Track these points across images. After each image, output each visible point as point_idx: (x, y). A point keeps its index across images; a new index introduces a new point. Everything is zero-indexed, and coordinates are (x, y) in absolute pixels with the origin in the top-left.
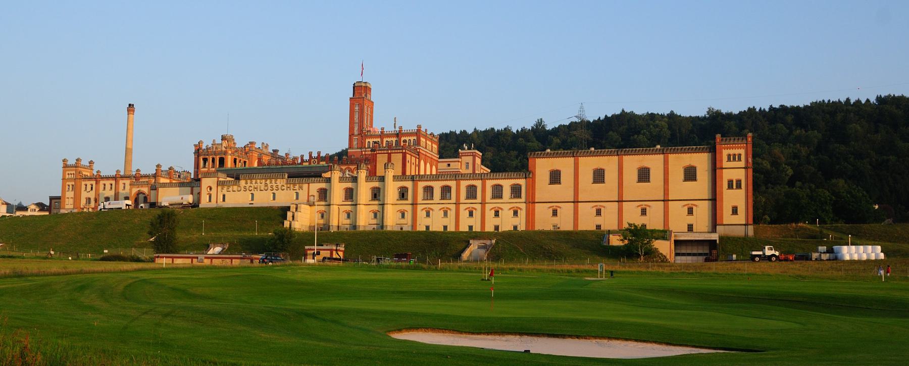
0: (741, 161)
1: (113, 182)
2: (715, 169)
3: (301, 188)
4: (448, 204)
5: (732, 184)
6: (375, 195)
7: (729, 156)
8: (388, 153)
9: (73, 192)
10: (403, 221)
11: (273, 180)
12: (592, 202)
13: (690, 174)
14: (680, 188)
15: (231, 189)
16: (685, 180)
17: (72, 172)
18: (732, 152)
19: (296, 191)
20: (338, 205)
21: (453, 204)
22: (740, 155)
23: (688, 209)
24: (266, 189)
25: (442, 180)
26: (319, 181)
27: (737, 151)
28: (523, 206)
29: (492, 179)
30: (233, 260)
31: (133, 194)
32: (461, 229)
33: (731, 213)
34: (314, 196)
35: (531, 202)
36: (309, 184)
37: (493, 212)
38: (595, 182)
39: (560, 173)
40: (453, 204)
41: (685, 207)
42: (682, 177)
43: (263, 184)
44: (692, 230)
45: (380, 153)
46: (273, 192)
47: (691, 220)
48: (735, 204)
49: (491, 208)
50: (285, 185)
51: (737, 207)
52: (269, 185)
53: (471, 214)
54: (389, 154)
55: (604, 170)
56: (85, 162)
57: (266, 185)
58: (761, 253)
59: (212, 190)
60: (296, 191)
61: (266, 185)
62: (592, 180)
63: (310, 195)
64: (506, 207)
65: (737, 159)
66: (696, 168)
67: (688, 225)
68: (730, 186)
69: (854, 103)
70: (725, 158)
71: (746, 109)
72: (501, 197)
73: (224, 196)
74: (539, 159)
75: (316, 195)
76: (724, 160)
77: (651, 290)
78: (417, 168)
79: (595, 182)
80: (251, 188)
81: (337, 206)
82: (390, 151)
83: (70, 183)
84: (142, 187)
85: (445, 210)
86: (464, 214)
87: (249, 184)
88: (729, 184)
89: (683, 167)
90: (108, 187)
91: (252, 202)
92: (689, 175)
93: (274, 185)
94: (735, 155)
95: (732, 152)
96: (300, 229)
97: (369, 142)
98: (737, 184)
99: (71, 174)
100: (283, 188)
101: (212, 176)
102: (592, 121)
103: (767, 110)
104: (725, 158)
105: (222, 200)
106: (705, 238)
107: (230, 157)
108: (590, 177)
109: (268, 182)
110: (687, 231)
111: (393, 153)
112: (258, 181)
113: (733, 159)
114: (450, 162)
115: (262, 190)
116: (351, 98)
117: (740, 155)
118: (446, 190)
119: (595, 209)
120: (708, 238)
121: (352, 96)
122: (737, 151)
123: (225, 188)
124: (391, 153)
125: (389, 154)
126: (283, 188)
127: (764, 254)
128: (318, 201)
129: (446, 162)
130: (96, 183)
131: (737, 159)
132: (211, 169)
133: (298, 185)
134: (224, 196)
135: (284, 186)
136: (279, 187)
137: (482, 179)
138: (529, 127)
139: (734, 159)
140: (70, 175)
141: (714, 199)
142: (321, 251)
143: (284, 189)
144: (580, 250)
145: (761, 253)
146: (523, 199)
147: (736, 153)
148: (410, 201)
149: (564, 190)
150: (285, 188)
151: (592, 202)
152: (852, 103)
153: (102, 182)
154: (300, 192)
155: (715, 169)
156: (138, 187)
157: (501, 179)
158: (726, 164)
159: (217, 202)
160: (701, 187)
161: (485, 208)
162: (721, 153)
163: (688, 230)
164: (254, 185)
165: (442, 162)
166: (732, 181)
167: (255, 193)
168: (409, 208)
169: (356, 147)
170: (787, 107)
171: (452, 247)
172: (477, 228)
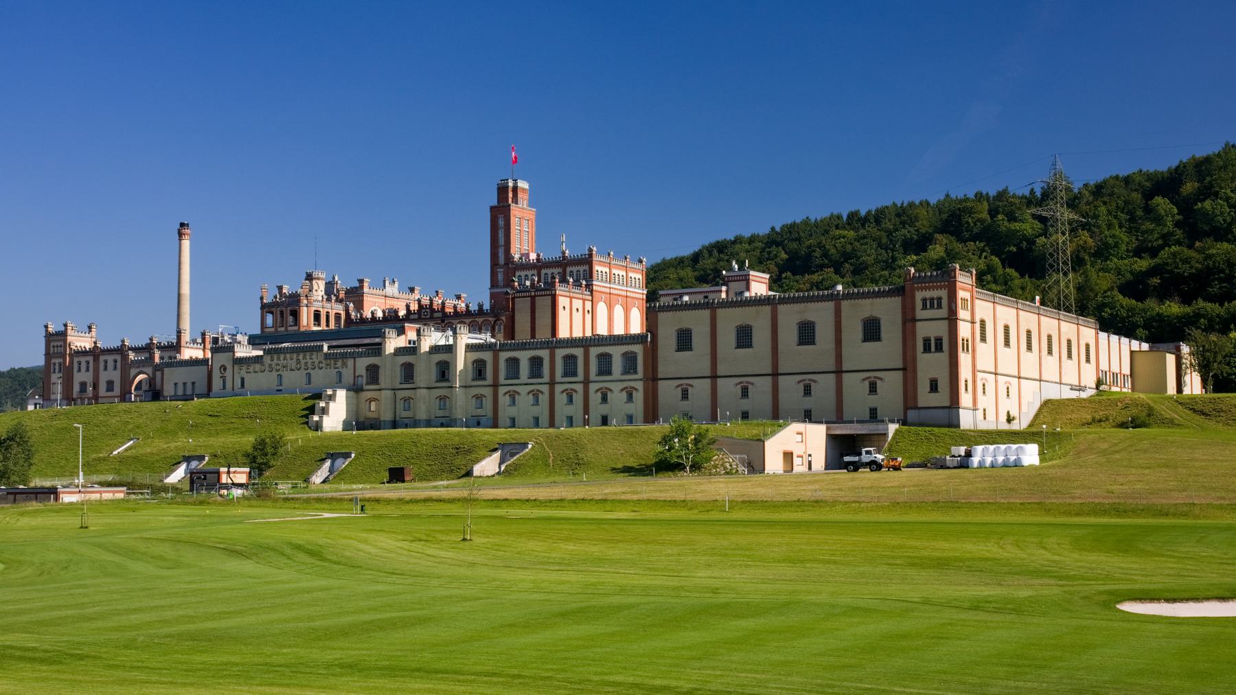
0: (942, 308)
1: (118, 358)
2: (909, 320)
3: (344, 365)
4: (539, 384)
5: (930, 344)
7: (924, 300)
8: (531, 296)
10: (480, 412)
11: (308, 354)
12: (736, 376)
13: (872, 331)
14: (858, 353)
15: (251, 369)
16: (865, 339)
17: (59, 344)
18: (928, 294)
19: (338, 370)
20: (394, 390)
21: (545, 384)
22: (940, 299)
23: (870, 384)
24: (263, 370)
25: (530, 349)
26: (369, 353)
27: (935, 294)
28: (639, 385)
29: (597, 346)
30: (38, 495)
33: (929, 390)
34: (362, 376)
35: (652, 378)
36: (355, 358)
37: (599, 394)
38: (739, 346)
40: (545, 384)
41: (865, 382)
42: (860, 336)
43: (295, 360)
44: (876, 417)
45: (519, 297)
46: (307, 371)
47: (873, 401)
48: (933, 376)
49: (622, 388)
50: (324, 361)
51: (937, 381)
52: (303, 362)
53: (570, 400)
54: (533, 298)
55: (751, 328)
57: (298, 361)
58: (856, 459)
59: (227, 371)
60: (338, 370)
61: (298, 361)
62: (734, 344)
63: (357, 374)
64: (616, 387)
65: (936, 306)
66: (879, 320)
67: (870, 409)
68: (927, 349)
72: (609, 373)
73: (243, 379)
75: (365, 375)
77: (908, 505)
78: (588, 317)
79: (739, 346)
80: (278, 367)
81: (393, 392)
82: (533, 294)
84: (143, 366)
85: (569, 393)
86: (561, 399)
87: (275, 361)
88: (925, 345)
89: (861, 321)
90: (110, 365)
92: (870, 330)
93: (310, 361)
95: (928, 294)
96: (336, 427)
97: (546, 274)
98: (936, 344)
100: (321, 365)
104: (919, 304)
105: (240, 386)
106: (870, 430)
107: (305, 309)
108: (673, 342)
109: (301, 357)
110: (868, 419)
111: (538, 296)
112: (288, 356)
113: (931, 306)
114: (708, 292)
115: (293, 370)
116: (492, 208)
117: (940, 299)
118: (536, 363)
119: (801, 385)
120: (873, 430)
121: (495, 203)
122: (935, 294)
123: (244, 368)
124: (535, 296)
125: (533, 298)
126: (321, 365)
127: (860, 460)
128: (368, 384)
129: (702, 292)
130: (94, 360)
131: (936, 306)
132: (279, 329)
133: (340, 361)
134: (243, 379)
135: (322, 363)
136: (316, 364)
137: (583, 346)
138: (659, 261)
139: (932, 307)
140: (56, 348)
141: (908, 369)
142: (207, 475)
143: (322, 368)
144: (1168, 417)
145: (856, 459)
146: (640, 375)
148: (489, 381)
149: (696, 359)
150: (323, 365)
151: (736, 376)
153: (102, 358)
154: (344, 371)
155: (909, 320)
156: (139, 367)
157: (610, 345)
158: (920, 313)
159: (233, 390)
160: (888, 349)
162: (913, 297)
163: (871, 418)
164: (282, 362)
165: (715, 291)
166: (930, 340)
167: (284, 373)
168: (488, 392)
169: (501, 284)
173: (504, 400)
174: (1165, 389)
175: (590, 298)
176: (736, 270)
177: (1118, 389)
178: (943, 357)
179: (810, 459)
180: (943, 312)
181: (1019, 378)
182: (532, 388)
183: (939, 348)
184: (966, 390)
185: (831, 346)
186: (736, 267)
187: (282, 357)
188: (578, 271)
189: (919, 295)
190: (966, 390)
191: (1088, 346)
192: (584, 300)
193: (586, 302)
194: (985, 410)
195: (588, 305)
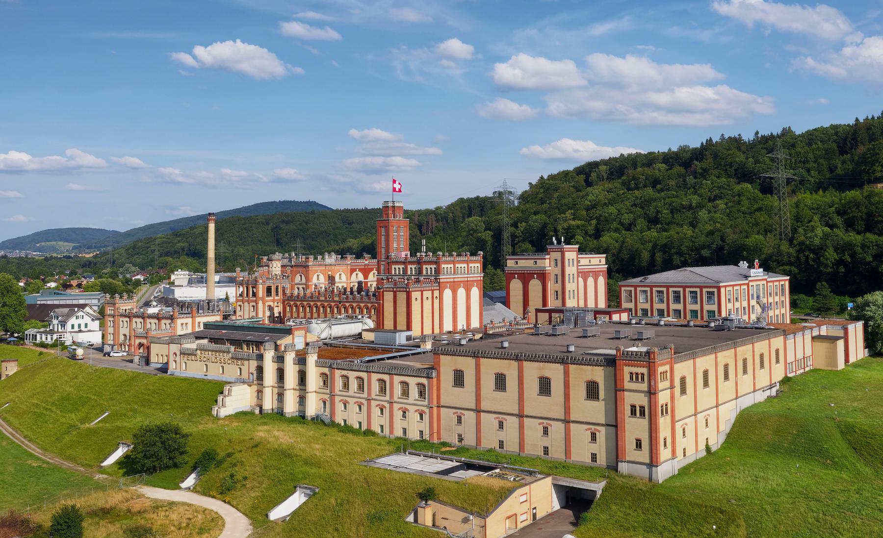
6: (421, 392)
18: (635, 370)
19: (238, 366)
32: (529, 450)
39: (598, 386)
47: (546, 442)
51: (641, 441)
68: (633, 412)
70: (627, 377)
74: (527, 362)
78: (437, 302)
82: (395, 289)
86: (376, 411)
94: (637, 374)
95: (635, 370)
104: (627, 377)
141: (614, 425)
147: (634, 372)
150: (230, 362)
158: (628, 385)
160: (596, 411)
161: (393, 408)
166: (635, 407)
172: (557, 453)
173: (339, 406)
174: (836, 365)
175: (438, 288)
176: (555, 244)
177: (802, 371)
178: (645, 422)
179: (534, 511)
180: (644, 386)
181: (717, 407)
182: (358, 400)
183: (642, 414)
184: (665, 445)
185: (562, 399)
186: (555, 242)
187: (207, 353)
188: (431, 268)
189: (627, 370)
190: (665, 445)
191: (777, 351)
192: (433, 291)
193: (435, 291)
194: (684, 449)
195: (436, 293)
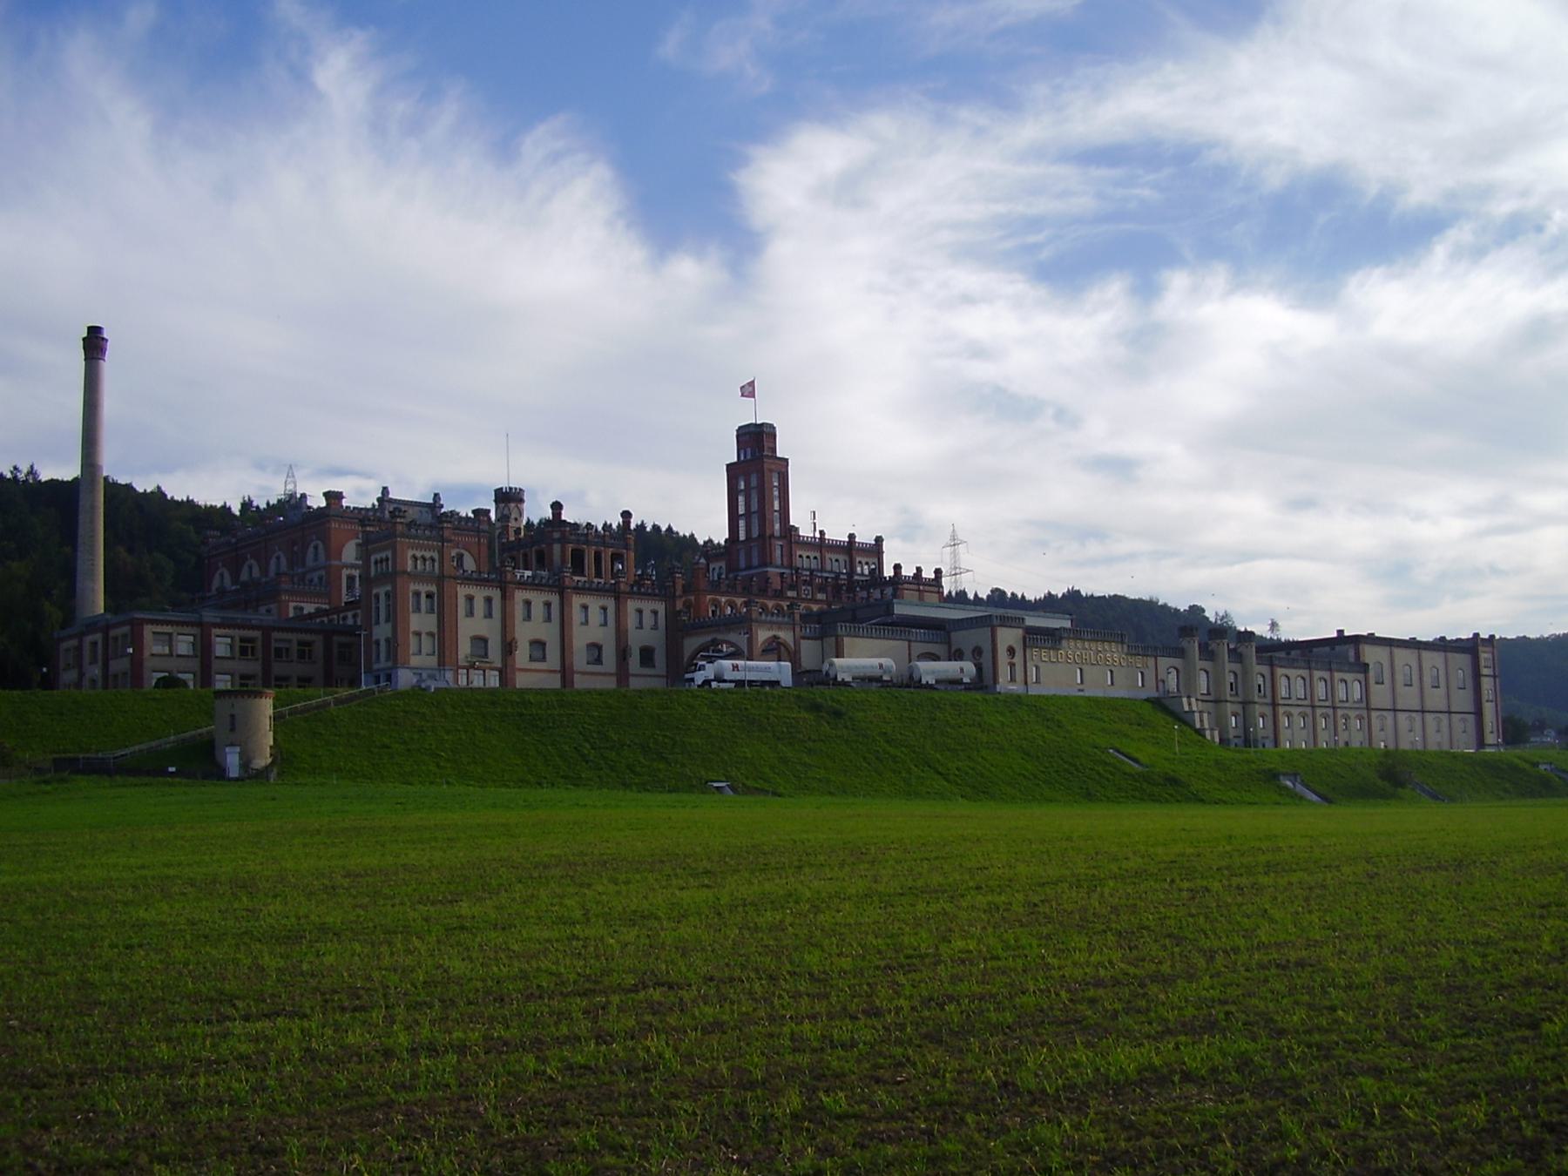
9: (390, 624)
17: (428, 555)
27: (462, 602)
31: (685, 660)
56: (928, 574)
69: (240, 511)
71: (219, 505)
76: (574, 623)
83: (424, 588)
91: (1081, 687)
99: (424, 559)
101: (1013, 624)
102: (1060, 596)
103: (236, 509)
152: (238, 513)
170: (1177, 610)
171: (846, 963)
